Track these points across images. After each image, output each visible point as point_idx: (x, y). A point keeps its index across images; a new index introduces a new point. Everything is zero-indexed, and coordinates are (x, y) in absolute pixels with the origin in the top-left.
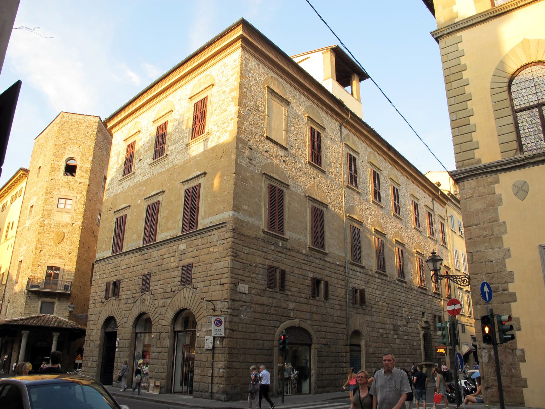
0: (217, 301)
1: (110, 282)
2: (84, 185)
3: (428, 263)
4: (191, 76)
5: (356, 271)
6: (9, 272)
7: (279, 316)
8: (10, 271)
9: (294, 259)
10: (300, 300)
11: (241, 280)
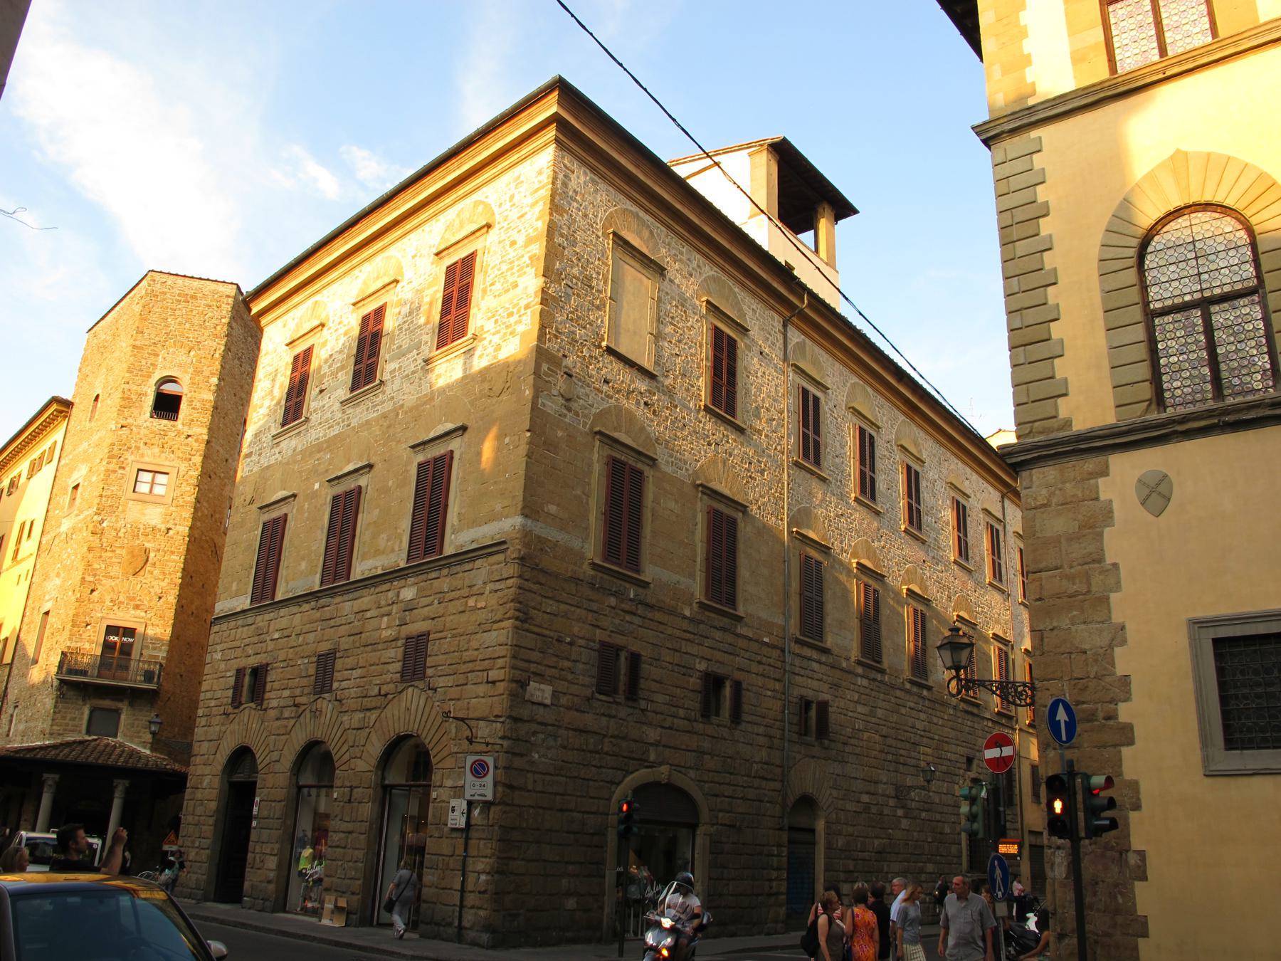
0: (478, 719)
1: (245, 668)
2: (197, 441)
3: (942, 652)
4: (442, 204)
5: (809, 659)
6: (18, 636)
7: (621, 759)
8: (21, 635)
9: (661, 627)
10: (673, 723)
11: (535, 674)
